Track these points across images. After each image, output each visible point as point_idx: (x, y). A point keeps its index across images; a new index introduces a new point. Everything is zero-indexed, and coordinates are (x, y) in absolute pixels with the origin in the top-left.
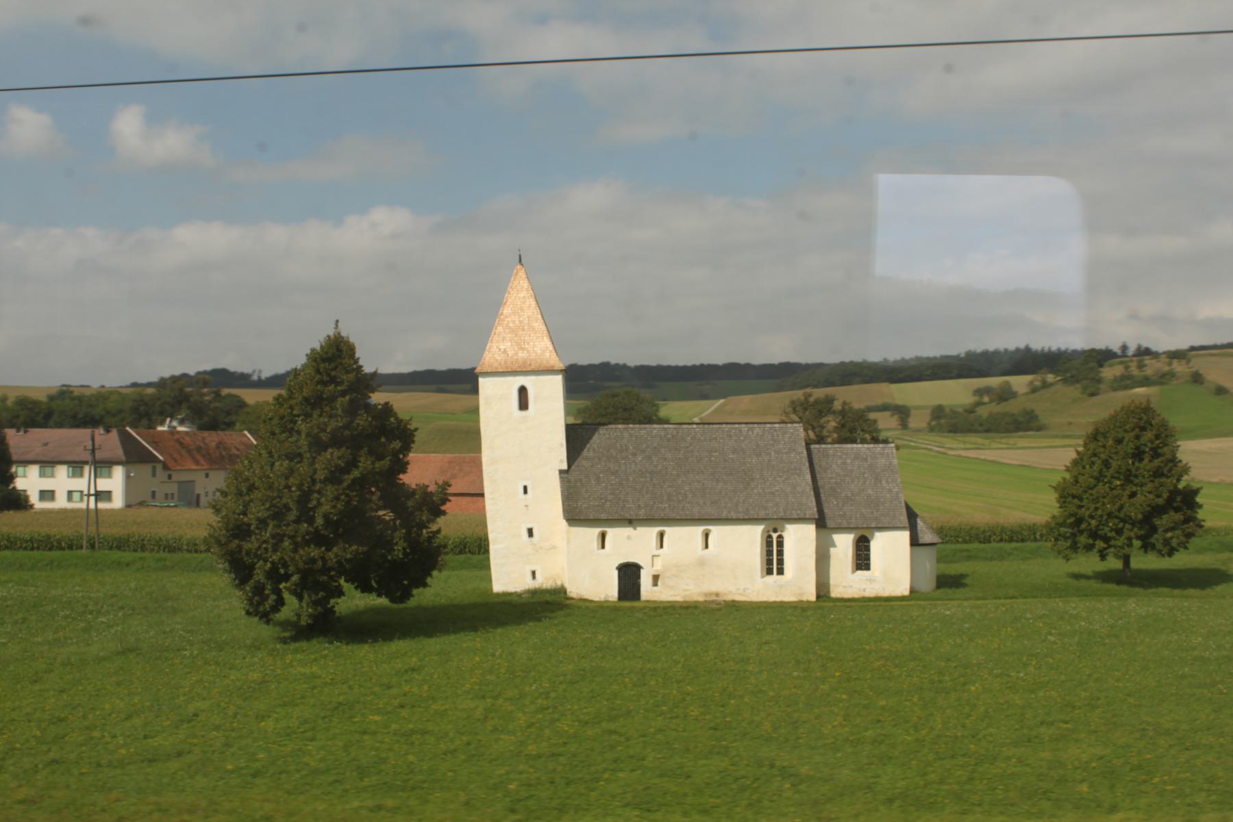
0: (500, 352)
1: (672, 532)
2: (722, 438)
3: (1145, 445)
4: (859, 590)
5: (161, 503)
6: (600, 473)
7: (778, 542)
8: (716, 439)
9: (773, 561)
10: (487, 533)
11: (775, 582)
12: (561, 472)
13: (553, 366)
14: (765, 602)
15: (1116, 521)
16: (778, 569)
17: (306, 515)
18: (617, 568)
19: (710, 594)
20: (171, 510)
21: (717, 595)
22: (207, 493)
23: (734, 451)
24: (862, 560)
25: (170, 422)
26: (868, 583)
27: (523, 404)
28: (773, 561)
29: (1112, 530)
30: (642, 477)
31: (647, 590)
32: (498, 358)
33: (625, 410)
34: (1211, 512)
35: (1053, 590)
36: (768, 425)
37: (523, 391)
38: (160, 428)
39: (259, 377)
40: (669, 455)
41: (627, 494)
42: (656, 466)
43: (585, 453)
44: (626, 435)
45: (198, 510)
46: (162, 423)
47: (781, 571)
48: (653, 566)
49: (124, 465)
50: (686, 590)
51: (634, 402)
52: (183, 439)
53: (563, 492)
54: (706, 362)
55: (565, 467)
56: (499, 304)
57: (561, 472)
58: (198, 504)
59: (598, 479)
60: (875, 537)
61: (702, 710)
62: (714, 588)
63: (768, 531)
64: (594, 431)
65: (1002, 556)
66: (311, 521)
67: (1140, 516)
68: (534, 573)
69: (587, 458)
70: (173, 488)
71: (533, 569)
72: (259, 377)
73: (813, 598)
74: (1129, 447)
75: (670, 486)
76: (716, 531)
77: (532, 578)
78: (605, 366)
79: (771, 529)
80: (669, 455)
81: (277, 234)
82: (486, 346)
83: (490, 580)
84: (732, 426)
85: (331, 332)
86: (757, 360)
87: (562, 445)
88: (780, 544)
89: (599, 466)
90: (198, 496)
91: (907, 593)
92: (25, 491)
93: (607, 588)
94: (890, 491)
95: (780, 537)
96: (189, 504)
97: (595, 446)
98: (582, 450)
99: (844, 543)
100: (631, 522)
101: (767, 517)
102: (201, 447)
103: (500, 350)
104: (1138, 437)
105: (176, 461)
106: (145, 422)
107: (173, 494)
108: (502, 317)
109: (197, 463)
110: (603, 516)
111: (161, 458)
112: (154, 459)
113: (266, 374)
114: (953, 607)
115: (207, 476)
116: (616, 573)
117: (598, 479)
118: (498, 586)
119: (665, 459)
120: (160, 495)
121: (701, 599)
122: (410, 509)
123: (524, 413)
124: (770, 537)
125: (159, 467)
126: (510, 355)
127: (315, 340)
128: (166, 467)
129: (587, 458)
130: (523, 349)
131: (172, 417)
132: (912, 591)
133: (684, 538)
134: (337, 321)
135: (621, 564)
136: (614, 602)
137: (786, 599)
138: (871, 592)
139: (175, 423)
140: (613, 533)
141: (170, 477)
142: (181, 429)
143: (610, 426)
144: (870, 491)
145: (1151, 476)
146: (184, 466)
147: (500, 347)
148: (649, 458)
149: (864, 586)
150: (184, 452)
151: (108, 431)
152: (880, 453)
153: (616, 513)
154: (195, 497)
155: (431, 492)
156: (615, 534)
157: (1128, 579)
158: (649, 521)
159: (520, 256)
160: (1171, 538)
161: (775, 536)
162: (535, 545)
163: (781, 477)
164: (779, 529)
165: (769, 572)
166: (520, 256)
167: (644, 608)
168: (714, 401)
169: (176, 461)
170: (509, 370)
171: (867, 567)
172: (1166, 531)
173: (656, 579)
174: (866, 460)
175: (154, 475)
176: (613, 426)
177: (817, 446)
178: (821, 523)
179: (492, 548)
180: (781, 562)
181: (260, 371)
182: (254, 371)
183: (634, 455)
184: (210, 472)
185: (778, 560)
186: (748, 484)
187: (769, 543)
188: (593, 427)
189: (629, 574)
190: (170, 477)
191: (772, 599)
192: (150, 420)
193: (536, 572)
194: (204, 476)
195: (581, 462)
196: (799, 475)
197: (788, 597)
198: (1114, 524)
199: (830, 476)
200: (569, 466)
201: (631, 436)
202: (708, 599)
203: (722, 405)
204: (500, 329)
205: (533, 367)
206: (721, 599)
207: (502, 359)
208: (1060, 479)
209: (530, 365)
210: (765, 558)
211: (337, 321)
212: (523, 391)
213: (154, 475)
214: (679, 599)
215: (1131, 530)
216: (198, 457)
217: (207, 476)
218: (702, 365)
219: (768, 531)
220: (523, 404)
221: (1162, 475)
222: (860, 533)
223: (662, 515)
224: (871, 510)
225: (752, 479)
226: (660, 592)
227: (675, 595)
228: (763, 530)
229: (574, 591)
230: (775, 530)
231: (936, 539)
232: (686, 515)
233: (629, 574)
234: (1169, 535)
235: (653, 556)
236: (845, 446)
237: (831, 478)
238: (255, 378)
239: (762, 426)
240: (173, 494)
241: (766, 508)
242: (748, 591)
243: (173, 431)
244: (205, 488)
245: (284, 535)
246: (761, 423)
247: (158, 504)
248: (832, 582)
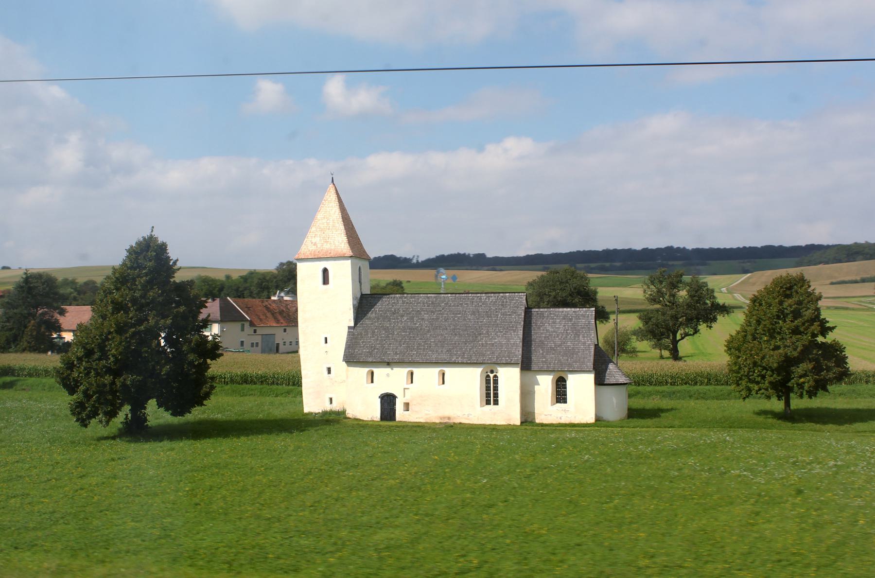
0: (312, 245)
1: (418, 372)
2: (466, 304)
3: (787, 309)
4: (557, 418)
5: (234, 350)
6: (376, 329)
7: (494, 380)
8: (462, 304)
9: (491, 395)
10: (300, 371)
11: (490, 410)
12: (349, 328)
13: (345, 254)
14: (483, 425)
15: (760, 368)
16: (494, 400)
17: (104, 356)
18: (379, 397)
19: (444, 418)
20: (241, 354)
21: (449, 418)
22: (285, 342)
23: (473, 313)
24: (560, 395)
25: (279, 293)
26: (564, 413)
27: (326, 281)
28: (491, 395)
29: (758, 376)
30: (404, 332)
31: (401, 414)
32: (310, 249)
33: (561, 283)
34: (855, 363)
35: (729, 424)
36: (501, 295)
37: (325, 271)
38: (273, 298)
39: (417, 261)
40: (426, 316)
41: (390, 344)
42: (416, 324)
43: (369, 315)
44: (400, 301)
45: (278, 355)
46: (275, 294)
47: (496, 403)
48: (404, 397)
49: (219, 324)
50: (427, 414)
51: (569, 277)
52: (270, 305)
53: (347, 342)
54: (593, 249)
55: (352, 324)
56: (315, 210)
57: (349, 328)
58: (277, 351)
59: (373, 332)
60: (569, 378)
61: (589, 507)
62: (447, 413)
63: (487, 372)
64: (380, 298)
65: (704, 397)
66: (107, 359)
67: (775, 365)
68: (331, 399)
69: (370, 318)
70: (257, 339)
71: (331, 397)
72: (417, 261)
73: (518, 422)
74: (774, 310)
75: (421, 339)
76: (449, 371)
77: (329, 403)
78: (670, 249)
79: (489, 371)
80: (426, 316)
81: (438, 159)
82: (304, 240)
83: (301, 402)
84: (475, 295)
85: (146, 233)
86: (788, 243)
87: (350, 309)
88: (496, 382)
89: (376, 324)
90: (278, 344)
91: (590, 418)
92: (834, 341)
93: (372, 412)
94: (584, 343)
95: (495, 376)
96: (270, 351)
97: (377, 310)
98: (368, 312)
99: (545, 384)
100: (388, 364)
101: (484, 362)
102: (283, 311)
103: (312, 243)
104: (781, 303)
105: (261, 320)
106: (265, 293)
107: (257, 344)
108: (316, 220)
109: (278, 321)
110: (370, 360)
111: (249, 319)
112: (243, 319)
113: (422, 259)
114: (643, 430)
115: (285, 330)
116: (379, 400)
117: (373, 332)
118: (306, 410)
119: (423, 319)
120: (247, 346)
121: (437, 421)
122: (185, 352)
123: (325, 286)
124: (488, 376)
125: (247, 325)
126: (318, 247)
127: (133, 238)
128: (252, 324)
129: (370, 318)
130: (327, 242)
131: (282, 290)
132: (598, 419)
133: (427, 375)
134: (153, 227)
135: (382, 394)
136: (378, 421)
137: (498, 423)
138: (565, 420)
139: (282, 294)
140: (379, 372)
141: (255, 331)
142: (286, 298)
143: (391, 296)
144: (569, 344)
145: (790, 333)
146: (267, 324)
147: (313, 241)
148: (412, 318)
149: (560, 415)
150: (269, 315)
151: (214, 300)
152: (582, 315)
153: (379, 357)
154: (275, 345)
155: (68, 342)
156: (380, 372)
157: (789, 416)
158: (401, 363)
159: (333, 178)
160: (804, 383)
161: (492, 376)
162: (332, 379)
163: (501, 332)
164: (495, 371)
165: (488, 403)
166: (333, 178)
167: (397, 427)
168: (744, 275)
169: (261, 320)
170: (316, 257)
171: (565, 402)
172: (801, 377)
173: (407, 406)
174: (571, 320)
175: (243, 330)
176: (393, 296)
177: (537, 310)
178: (526, 366)
179: (304, 381)
180: (496, 395)
181: (418, 257)
182: (414, 257)
183: (402, 316)
184: (288, 329)
185: (494, 394)
186: (476, 337)
187: (488, 381)
188: (379, 296)
189: (388, 401)
190: (255, 331)
191: (488, 423)
192: (269, 292)
193: (333, 399)
194: (283, 330)
195: (366, 321)
196: (514, 331)
197: (500, 421)
198: (759, 371)
199: (542, 332)
200: (356, 324)
201: (404, 302)
202: (442, 421)
203: (749, 278)
204: (313, 229)
205: (332, 255)
206: (451, 421)
207: (312, 250)
208: (827, 336)
209: (330, 253)
210: (484, 392)
211: (153, 227)
212: (325, 271)
213: (243, 330)
214: (422, 420)
215: (771, 376)
216: (280, 318)
217: (285, 330)
218: (781, 247)
219: (487, 372)
220: (326, 281)
221: (800, 333)
222: (558, 375)
223: (410, 359)
224: (566, 358)
225: (480, 334)
226: (409, 415)
227: (419, 418)
228: (482, 372)
229: (350, 413)
230: (492, 372)
231: (622, 380)
232: (427, 359)
233: (388, 401)
234: (802, 380)
235: (404, 389)
236: (557, 310)
237: (542, 334)
238: (414, 261)
239: (497, 295)
240: (257, 344)
241: (484, 355)
242: (471, 416)
243: (281, 299)
244: (283, 339)
245: (91, 368)
246: (496, 293)
247: (233, 350)
248: (536, 411)
